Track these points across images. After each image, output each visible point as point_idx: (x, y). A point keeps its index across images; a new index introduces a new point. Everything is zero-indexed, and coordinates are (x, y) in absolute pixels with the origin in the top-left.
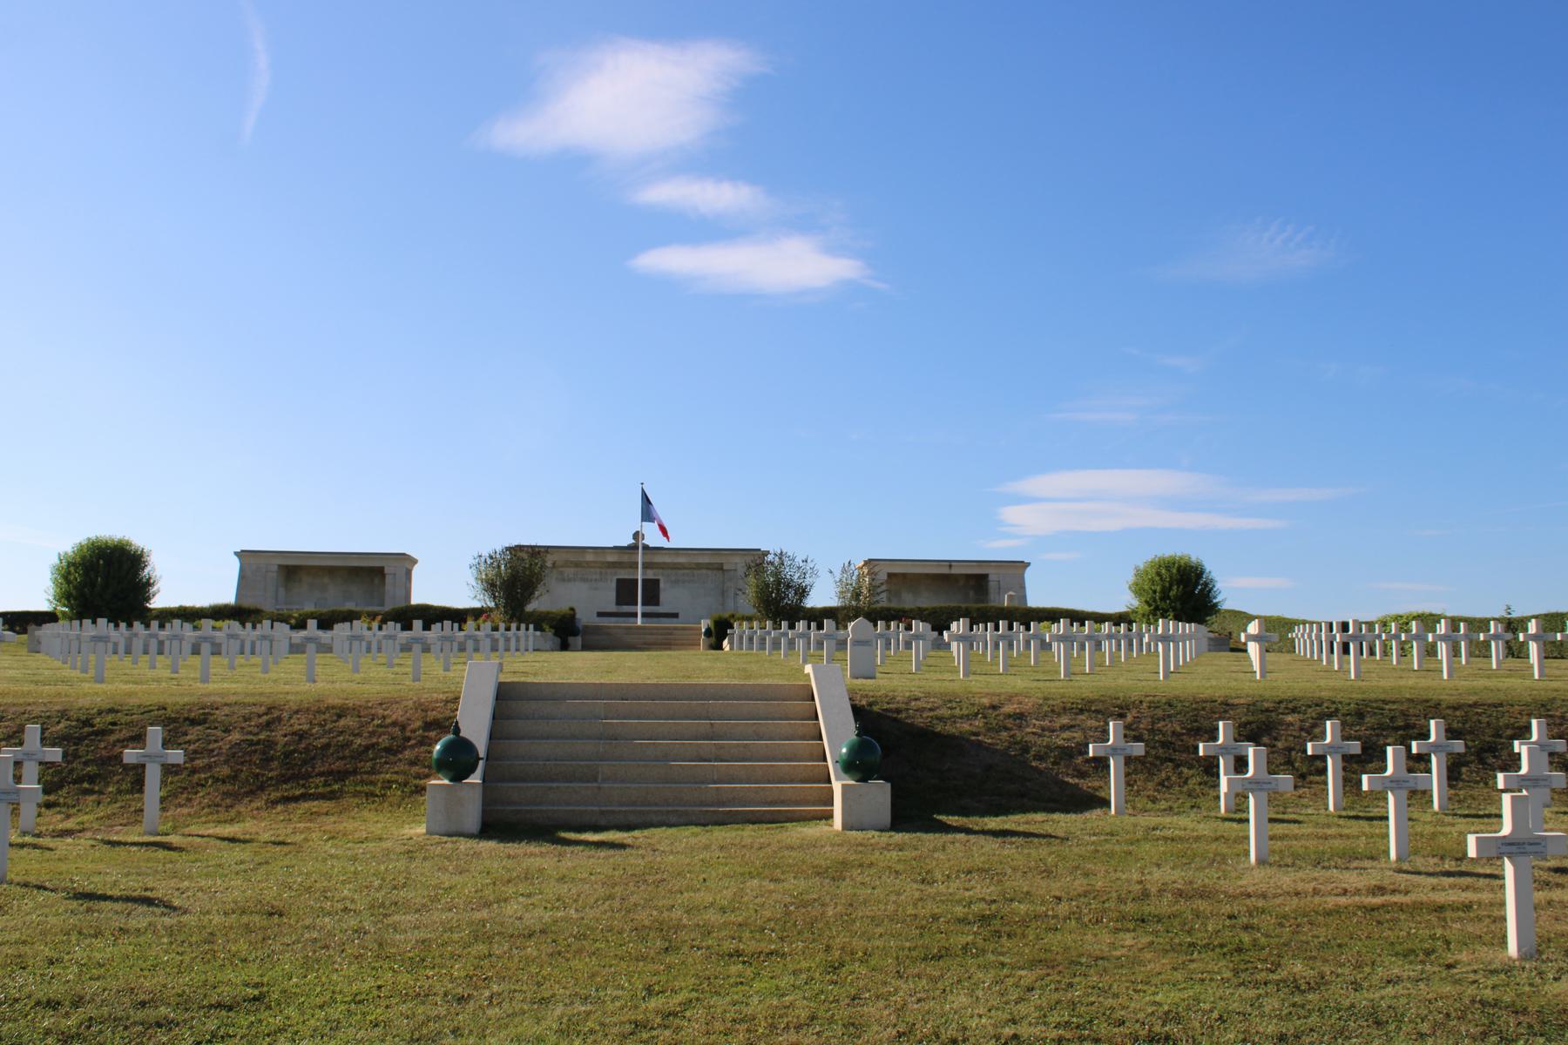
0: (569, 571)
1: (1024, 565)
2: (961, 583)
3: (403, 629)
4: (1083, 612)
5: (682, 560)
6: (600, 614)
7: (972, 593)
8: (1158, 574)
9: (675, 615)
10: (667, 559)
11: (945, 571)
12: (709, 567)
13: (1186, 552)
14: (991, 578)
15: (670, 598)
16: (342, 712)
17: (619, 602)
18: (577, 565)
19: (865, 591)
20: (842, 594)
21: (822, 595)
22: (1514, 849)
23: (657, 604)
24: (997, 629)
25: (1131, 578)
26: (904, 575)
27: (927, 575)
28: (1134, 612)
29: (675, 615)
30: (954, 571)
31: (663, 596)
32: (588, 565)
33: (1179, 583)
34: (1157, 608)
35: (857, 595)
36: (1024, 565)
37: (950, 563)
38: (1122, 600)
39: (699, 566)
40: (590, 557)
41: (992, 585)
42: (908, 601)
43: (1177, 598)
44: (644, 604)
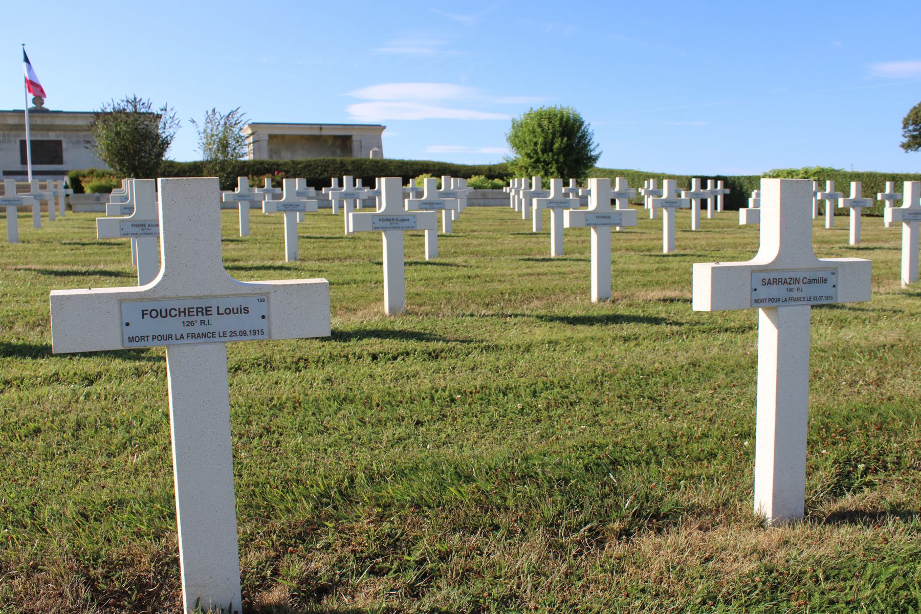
2: (330, 143)
3: (224, 188)
7: (338, 151)
8: (540, 126)
10: (67, 122)
11: (316, 132)
13: (565, 105)
14: (354, 138)
20: (207, 147)
22: (387, 224)
23: (61, 162)
24: (341, 184)
25: (508, 130)
26: (283, 137)
27: (302, 137)
28: (514, 163)
30: (325, 132)
31: (66, 156)
33: (562, 135)
34: (538, 161)
36: (380, 128)
37: (321, 127)
38: (497, 151)
41: (355, 144)
42: (286, 157)
43: (561, 150)
44: (33, 163)
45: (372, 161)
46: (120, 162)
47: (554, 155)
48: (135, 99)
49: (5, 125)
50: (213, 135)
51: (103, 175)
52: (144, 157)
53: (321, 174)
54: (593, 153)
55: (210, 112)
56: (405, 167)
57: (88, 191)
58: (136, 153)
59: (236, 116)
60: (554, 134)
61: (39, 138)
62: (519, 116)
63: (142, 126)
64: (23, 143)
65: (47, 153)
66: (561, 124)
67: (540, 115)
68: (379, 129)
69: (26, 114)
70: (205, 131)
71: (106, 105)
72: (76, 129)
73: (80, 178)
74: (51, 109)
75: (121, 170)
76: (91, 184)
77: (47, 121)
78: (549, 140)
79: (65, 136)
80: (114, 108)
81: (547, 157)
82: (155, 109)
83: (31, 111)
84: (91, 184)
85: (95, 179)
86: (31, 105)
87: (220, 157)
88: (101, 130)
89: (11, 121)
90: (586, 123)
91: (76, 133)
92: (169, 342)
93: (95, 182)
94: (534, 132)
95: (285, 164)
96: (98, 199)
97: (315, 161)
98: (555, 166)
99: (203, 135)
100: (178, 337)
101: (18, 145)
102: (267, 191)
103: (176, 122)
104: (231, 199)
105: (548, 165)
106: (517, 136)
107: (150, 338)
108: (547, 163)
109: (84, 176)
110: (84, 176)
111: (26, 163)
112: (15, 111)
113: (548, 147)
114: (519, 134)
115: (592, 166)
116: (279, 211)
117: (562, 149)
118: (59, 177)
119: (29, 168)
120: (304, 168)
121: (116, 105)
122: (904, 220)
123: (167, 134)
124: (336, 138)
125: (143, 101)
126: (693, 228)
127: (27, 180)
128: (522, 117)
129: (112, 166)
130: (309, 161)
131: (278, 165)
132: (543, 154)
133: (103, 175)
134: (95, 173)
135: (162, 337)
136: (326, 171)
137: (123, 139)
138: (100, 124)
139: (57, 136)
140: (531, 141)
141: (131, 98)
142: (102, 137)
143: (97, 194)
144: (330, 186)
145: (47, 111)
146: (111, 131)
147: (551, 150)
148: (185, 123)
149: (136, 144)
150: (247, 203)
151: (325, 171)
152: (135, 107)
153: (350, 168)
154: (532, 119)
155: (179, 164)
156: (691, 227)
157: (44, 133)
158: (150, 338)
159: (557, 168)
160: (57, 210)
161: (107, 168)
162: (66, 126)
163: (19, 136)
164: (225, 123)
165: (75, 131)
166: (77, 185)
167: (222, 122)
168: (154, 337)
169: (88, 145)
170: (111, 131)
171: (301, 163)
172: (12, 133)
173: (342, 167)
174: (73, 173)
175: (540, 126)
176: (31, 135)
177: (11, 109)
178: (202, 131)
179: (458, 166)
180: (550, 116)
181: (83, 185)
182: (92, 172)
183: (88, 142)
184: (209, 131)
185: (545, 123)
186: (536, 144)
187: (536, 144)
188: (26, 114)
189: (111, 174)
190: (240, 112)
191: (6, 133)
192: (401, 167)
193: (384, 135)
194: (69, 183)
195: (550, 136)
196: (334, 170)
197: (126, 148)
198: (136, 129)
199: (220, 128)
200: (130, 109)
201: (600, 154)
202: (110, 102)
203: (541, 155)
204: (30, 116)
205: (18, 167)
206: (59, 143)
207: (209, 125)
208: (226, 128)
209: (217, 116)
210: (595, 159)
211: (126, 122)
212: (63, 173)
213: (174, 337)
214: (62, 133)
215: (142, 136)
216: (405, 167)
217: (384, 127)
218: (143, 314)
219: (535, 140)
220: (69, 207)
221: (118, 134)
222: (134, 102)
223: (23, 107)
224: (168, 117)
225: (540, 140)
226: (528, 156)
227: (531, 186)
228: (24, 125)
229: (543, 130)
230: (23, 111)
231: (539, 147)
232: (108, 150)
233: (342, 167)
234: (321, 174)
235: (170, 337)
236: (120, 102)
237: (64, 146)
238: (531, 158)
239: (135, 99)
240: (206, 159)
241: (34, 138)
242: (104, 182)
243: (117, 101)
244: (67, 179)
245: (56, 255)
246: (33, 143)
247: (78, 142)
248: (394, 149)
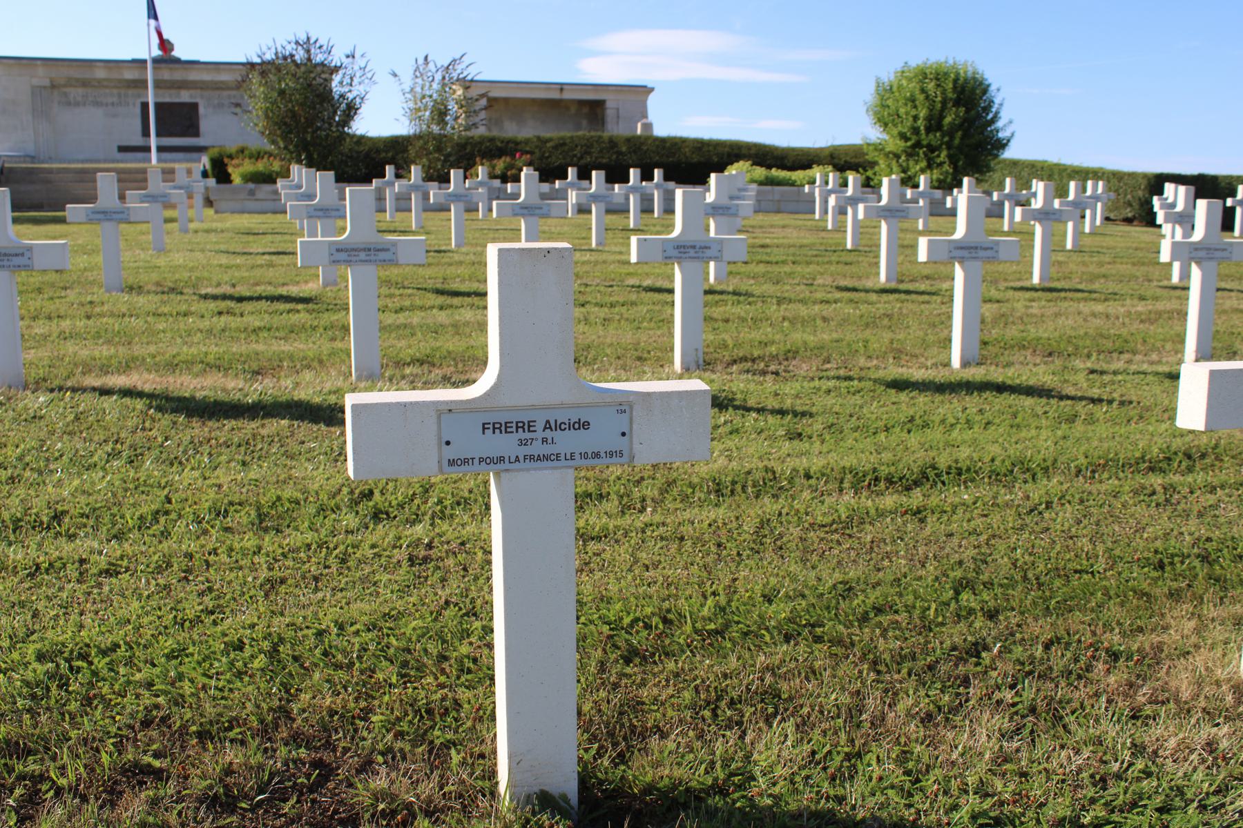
0: (76, 93)
2: (573, 110)
4: (701, 146)
6: (122, 149)
7: (584, 123)
8: (923, 91)
10: (206, 77)
11: (555, 95)
14: (608, 104)
16: (509, 142)
18: (85, 83)
19: (453, 107)
20: (415, 114)
21: (381, 116)
23: (196, 134)
25: (868, 94)
27: (534, 101)
28: (879, 148)
30: (567, 95)
31: (204, 125)
32: (100, 84)
33: (957, 103)
34: (918, 145)
35: (440, 114)
36: (645, 91)
37: (561, 87)
38: (856, 128)
40: (101, 74)
41: (610, 113)
42: (511, 130)
44: (158, 135)
45: (640, 137)
46: (285, 137)
47: (943, 136)
48: (308, 39)
49: (120, 81)
50: (424, 97)
51: (258, 156)
52: (319, 128)
53: (582, 158)
54: (1000, 135)
55: (421, 61)
56: (705, 149)
57: (237, 179)
58: (310, 122)
59: (459, 68)
60: (944, 102)
61: (167, 100)
62: (888, 74)
63: (319, 80)
64: (145, 106)
65: (178, 121)
66: (955, 88)
67: (922, 75)
68: (643, 91)
69: (149, 65)
70: (412, 90)
71: (264, 49)
73: (226, 160)
74: (184, 57)
75: (286, 148)
76: (241, 170)
77: (178, 75)
78: (936, 112)
79: (202, 97)
80: (276, 54)
81: (935, 138)
82: (336, 58)
83: (156, 61)
84: (241, 170)
85: (247, 161)
86: (157, 52)
87: (435, 129)
88: (256, 85)
89: (129, 75)
90: (993, 88)
91: (218, 92)
92: (501, 466)
93: (248, 167)
94: (913, 100)
95: (527, 141)
96: (252, 193)
97: (572, 138)
98: (944, 154)
99: (409, 96)
100: (513, 460)
101: (138, 110)
102: (572, 185)
103: (369, 75)
104: (404, 190)
105: (933, 152)
106: (884, 106)
107: (476, 461)
108: (931, 149)
109: (231, 157)
110: (231, 157)
111: (149, 135)
112: (134, 61)
113: (934, 123)
114: (890, 102)
115: (997, 156)
116: (515, 215)
117: (952, 129)
118: (195, 155)
119: (153, 142)
120: (556, 147)
121: (280, 49)
122: (1035, 219)
123: (354, 94)
124: (582, 103)
125: (322, 41)
126: (830, 227)
127: (150, 161)
128: (892, 77)
129: (273, 142)
130: (562, 138)
131: (517, 143)
132: (927, 134)
133: (258, 156)
134: (246, 152)
135: (492, 460)
136: (589, 153)
137: (291, 101)
138: (255, 78)
139: (191, 96)
140: (907, 113)
141: (303, 38)
142: (257, 99)
143: (251, 186)
144: (627, 181)
145: (178, 61)
146: (273, 89)
147: (939, 127)
148: (382, 77)
149: (304, 113)
150: (461, 205)
151: (587, 153)
152: (308, 51)
153: (624, 149)
154: (910, 80)
155: (371, 139)
156: (1065, 246)
157: (173, 91)
158: (476, 461)
159: (949, 156)
160: (191, 207)
161: (259, 142)
162: (203, 82)
163: (139, 96)
164: (444, 78)
165: (218, 89)
166: (220, 171)
167: (438, 77)
168: (481, 460)
169: (238, 110)
170: (273, 89)
171: (550, 140)
172: (130, 92)
173: (612, 148)
174: (214, 152)
175: (923, 91)
176: (156, 95)
177: (129, 58)
178: (408, 89)
179: (783, 149)
180: (939, 76)
181: (230, 170)
182: (242, 151)
183: (238, 105)
184: (418, 89)
185: (931, 86)
186: (916, 118)
187: (916, 118)
188: (149, 65)
189: (270, 155)
190: (466, 60)
191: (123, 91)
192: (700, 149)
193: (652, 101)
194: (208, 167)
195: (939, 106)
196: (601, 151)
197: (294, 116)
198: (310, 85)
199: (435, 86)
200: (300, 55)
201: (1013, 135)
202: (271, 44)
203: (923, 136)
204: (154, 68)
205: (138, 141)
206: (194, 107)
207: (419, 81)
208: (444, 85)
209: (431, 66)
210: (1002, 145)
211: (294, 75)
212: (201, 149)
213: (507, 460)
214: (199, 91)
215: (318, 96)
216: (705, 149)
217: (652, 90)
218: (484, 428)
219: (914, 112)
220: (209, 203)
221: (282, 93)
222: (307, 45)
223: (143, 55)
224: (356, 68)
225: (923, 113)
226: (903, 136)
227: (827, 183)
228: (146, 81)
229: (927, 98)
230: (145, 61)
231: (921, 123)
232: (267, 117)
233: (612, 148)
234: (582, 158)
235: (501, 459)
236: (285, 44)
237: (201, 110)
238: (906, 139)
239: (308, 39)
240: (412, 132)
241: (161, 100)
242: (260, 166)
243: (281, 41)
244: (205, 161)
246: (158, 106)
247: (221, 106)
248: (669, 120)
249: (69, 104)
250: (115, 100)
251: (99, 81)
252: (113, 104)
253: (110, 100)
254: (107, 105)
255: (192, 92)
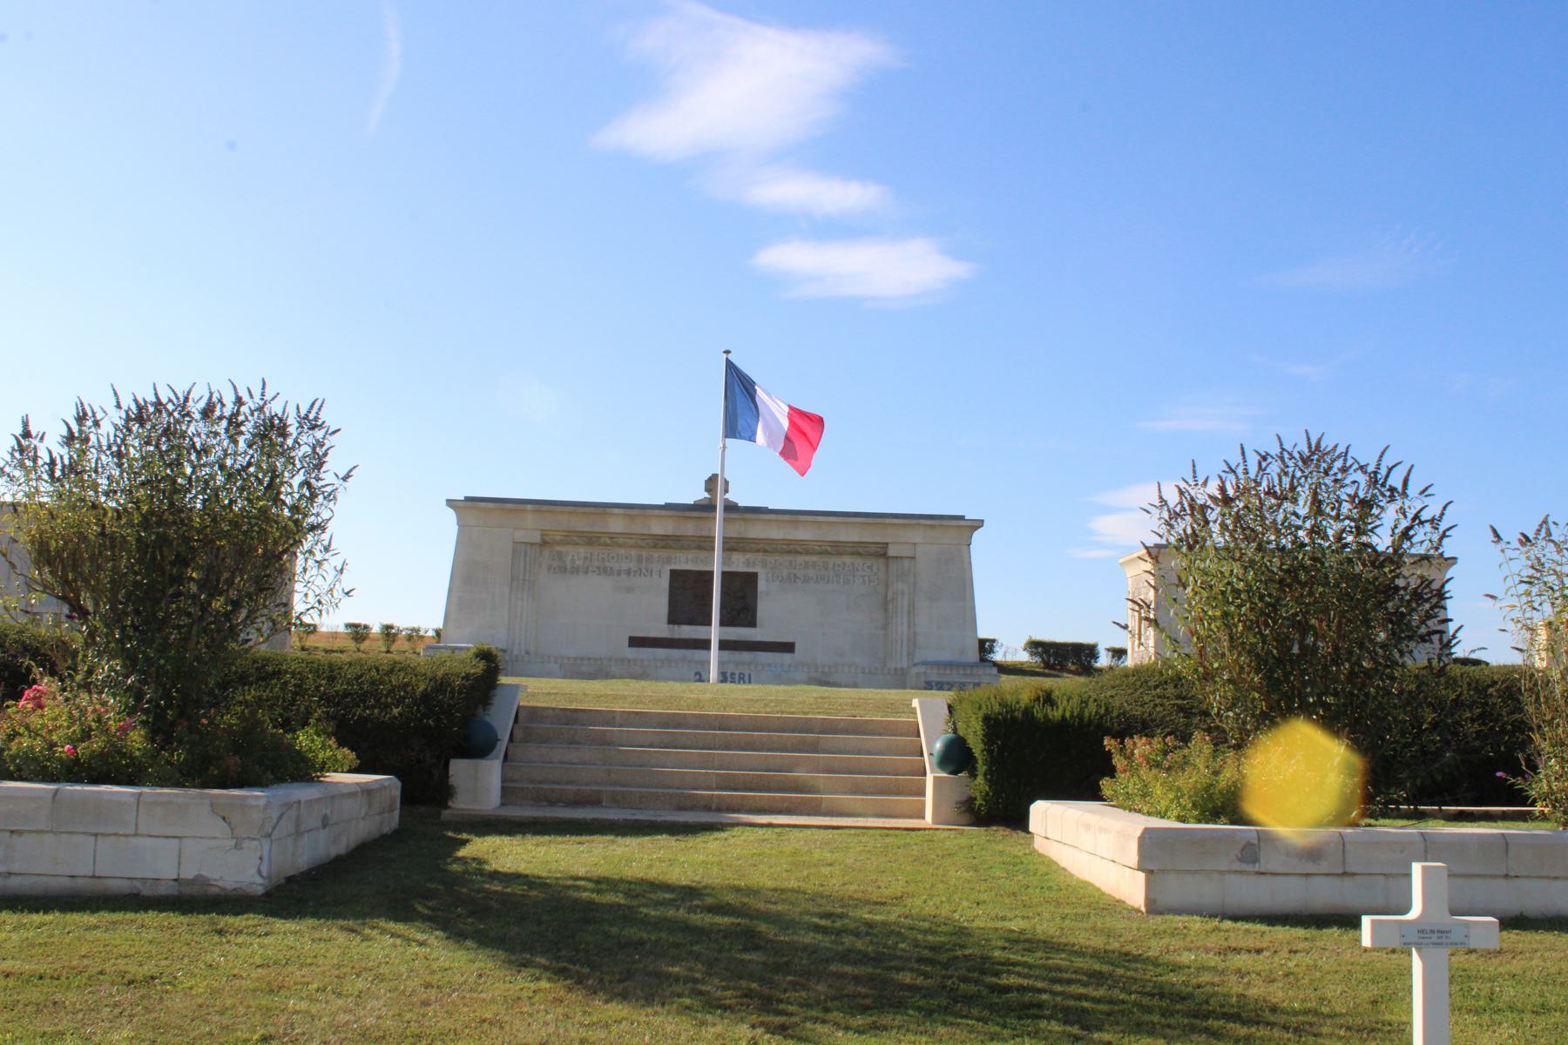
0: (576, 554)
1: (963, 527)
5: (803, 534)
6: (636, 642)
9: (788, 647)
10: (775, 533)
12: (858, 550)
15: (777, 611)
17: (673, 619)
29: (788, 647)
31: (764, 608)
32: (613, 540)
36: (963, 527)
39: (837, 549)
40: (617, 525)
49: (643, 537)
72: (791, 548)
74: (743, 502)
91: (790, 558)
112: (668, 507)
139: (748, 563)
163: (669, 561)
172: (656, 554)
176: (725, 561)
177: (660, 501)
192: (627, 976)
202: (1235, 460)
214: (760, 556)
217: (977, 524)
237: (762, 585)
245: (1136, 970)
249: (564, 570)
250: (633, 565)
251: (612, 536)
252: (628, 572)
253: (625, 566)
254: (619, 573)
255: (749, 556)
